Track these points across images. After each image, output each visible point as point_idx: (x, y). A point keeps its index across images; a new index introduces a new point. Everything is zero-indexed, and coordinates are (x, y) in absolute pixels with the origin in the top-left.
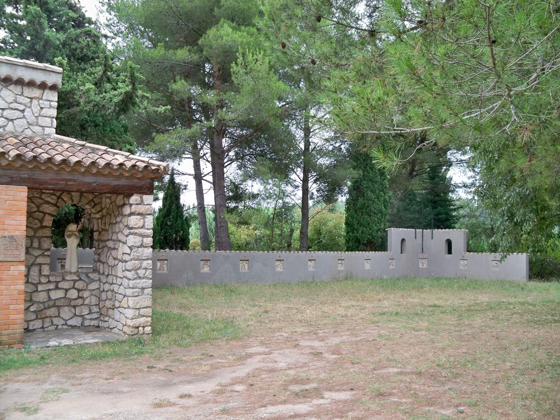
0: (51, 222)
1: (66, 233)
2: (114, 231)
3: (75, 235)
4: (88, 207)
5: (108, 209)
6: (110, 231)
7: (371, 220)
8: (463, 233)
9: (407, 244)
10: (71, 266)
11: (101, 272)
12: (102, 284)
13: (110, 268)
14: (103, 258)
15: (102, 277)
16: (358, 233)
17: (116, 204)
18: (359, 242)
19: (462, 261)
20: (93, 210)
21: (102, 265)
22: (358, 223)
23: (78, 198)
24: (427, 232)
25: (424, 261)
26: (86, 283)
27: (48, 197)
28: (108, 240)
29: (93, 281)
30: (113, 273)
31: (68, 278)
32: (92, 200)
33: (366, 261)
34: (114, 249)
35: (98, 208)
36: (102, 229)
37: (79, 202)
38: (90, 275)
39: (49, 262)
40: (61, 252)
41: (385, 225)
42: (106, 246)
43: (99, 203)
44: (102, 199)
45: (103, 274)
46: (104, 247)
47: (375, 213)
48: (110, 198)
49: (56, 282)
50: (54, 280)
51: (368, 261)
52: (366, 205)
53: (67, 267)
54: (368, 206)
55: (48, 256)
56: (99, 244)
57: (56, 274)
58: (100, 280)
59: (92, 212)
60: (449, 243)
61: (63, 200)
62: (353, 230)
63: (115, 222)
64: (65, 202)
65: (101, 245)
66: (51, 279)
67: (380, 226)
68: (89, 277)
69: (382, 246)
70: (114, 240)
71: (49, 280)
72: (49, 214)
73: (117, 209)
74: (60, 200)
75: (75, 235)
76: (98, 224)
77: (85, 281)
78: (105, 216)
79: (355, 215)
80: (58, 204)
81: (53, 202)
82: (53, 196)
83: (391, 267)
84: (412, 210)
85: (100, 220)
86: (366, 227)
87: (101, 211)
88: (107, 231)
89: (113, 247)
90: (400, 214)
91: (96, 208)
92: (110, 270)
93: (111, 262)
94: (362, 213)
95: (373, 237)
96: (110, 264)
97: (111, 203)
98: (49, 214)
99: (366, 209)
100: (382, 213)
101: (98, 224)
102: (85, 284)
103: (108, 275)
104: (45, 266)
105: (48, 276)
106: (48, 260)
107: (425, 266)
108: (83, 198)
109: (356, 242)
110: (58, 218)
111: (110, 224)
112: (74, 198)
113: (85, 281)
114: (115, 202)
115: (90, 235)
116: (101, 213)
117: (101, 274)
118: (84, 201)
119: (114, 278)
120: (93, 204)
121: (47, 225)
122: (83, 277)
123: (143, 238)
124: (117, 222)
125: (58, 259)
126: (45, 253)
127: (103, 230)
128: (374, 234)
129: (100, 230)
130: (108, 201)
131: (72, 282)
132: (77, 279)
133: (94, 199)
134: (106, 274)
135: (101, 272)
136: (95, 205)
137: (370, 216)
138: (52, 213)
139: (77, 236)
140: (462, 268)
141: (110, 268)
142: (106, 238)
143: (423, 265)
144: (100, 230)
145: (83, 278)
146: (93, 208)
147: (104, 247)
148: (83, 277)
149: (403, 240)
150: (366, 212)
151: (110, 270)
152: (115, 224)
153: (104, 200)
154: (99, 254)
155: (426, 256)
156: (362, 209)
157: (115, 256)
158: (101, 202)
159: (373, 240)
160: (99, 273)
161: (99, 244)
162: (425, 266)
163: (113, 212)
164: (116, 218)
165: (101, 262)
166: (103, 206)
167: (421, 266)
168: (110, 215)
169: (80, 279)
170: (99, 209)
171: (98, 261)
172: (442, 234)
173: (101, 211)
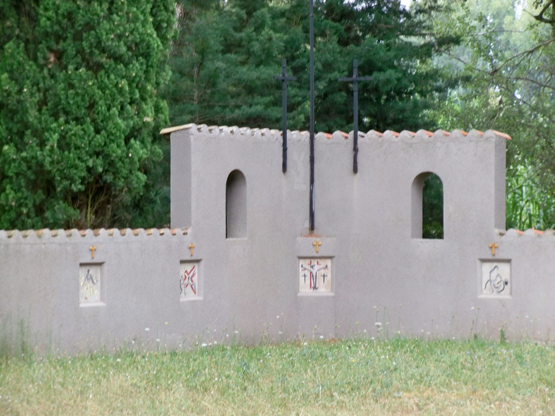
7: (102, 88)
8: (492, 146)
9: (252, 192)
16: (42, 144)
18: (49, 187)
19: (487, 267)
22: (43, 103)
24: (334, 143)
25: (318, 267)
33: (83, 272)
41: (158, 110)
47: (118, 58)
51: (93, 271)
52: (81, 19)
54: (89, 26)
60: (430, 189)
62: (21, 135)
67: (140, 113)
69: (147, 208)
79: (30, 67)
83: (188, 296)
84: (256, 47)
86: (77, 120)
90: (210, 66)
94: (59, 55)
95: (112, 164)
99: (78, 37)
100: (147, 56)
107: (324, 290)
109: (33, 186)
115: (536, 27)
125: (182, 262)
128: (116, 150)
137: (95, 68)
140: (486, 294)
143: (316, 285)
149: (234, 179)
150: (80, 52)
155: (327, 245)
156: (59, 38)
159: (109, 178)
162: (324, 290)
167: (305, 289)
172: (393, 157)
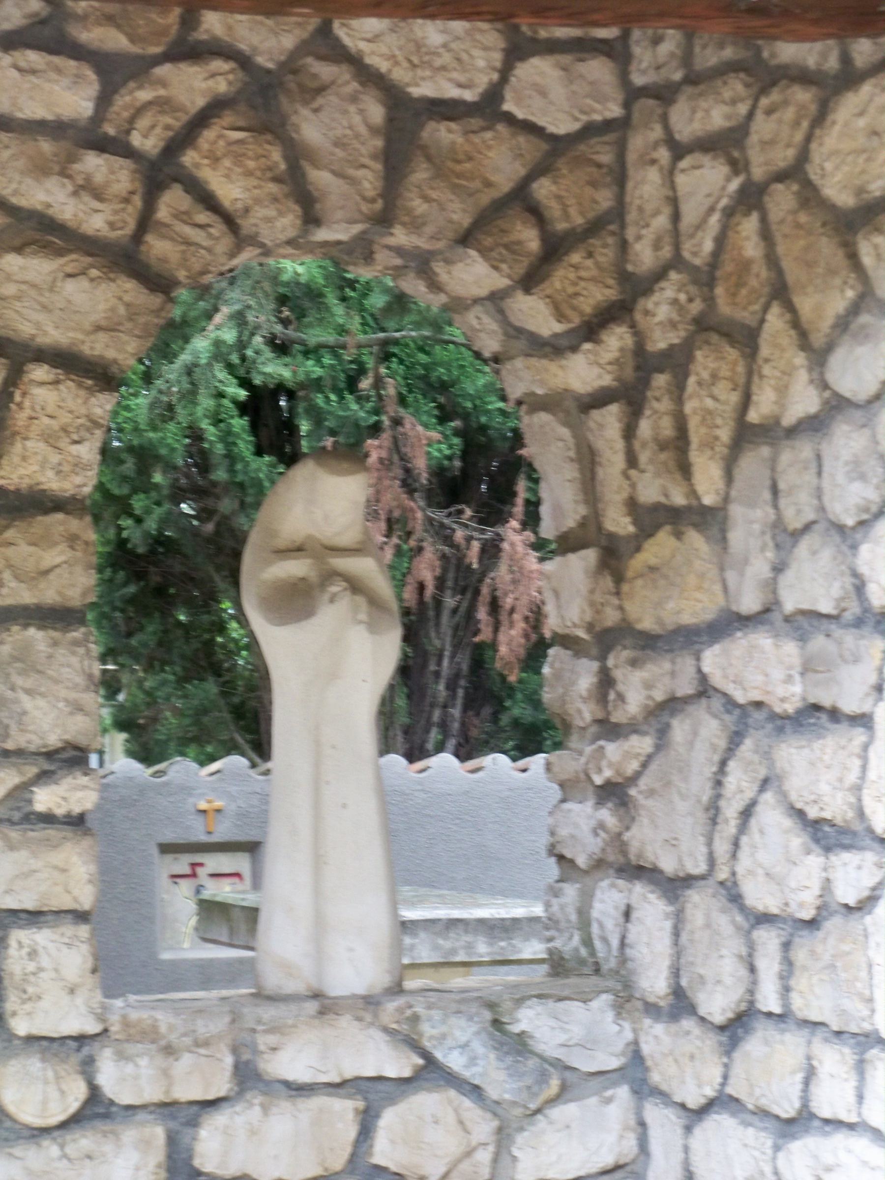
0: (88, 451)
1: (260, 572)
2: (797, 509)
3: (355, 586)
4: (473, 275)
5: (705, 279)
6: (747, 525)
10: (320, 928)
11: (655, 983)
12: (662, 1122)
13: (769, 941)
14: (668, 833)
15: (657, 1038)
17: (810, 196)
20: (535, 313)
21: (652, 909)
23: (370, 180)
26: (493, 1107)
27: (40, 169)
28: (728, 624)
29: (571, 1082)
30: (814, 999)
31: (293, 1061)
32: (520, 199)
34: (815, 716)
35: (585, 281)
36: (632, 505)
37: (384, 219)
38: (528, 1019)
39: (85, 896)
40: (187, 790)
42: (705, 689)
43: (595, 227)
44: (619, 177)
45: (680, 1004)
46: (672, 705)
48: (727, 144)
49: (167, 1108)
50: (152, 1093)
53: (284, 945)
55: (77, 822)
56: (606, 681)
57: (164, 1019)
58: (635, 1072)
59: (514, 332)
61: (208, 201)
63: (804, 401)
64: (229, 221)
65: (637, 688)
66: (116, 1078)
68: (518, 1046)
70: (806, 622)
71: (95, 1094)
72: (68, 362)
73: (828, 248)
74: (173, 201)
75: (355, 586)
76: (588, 460)
77: (475, 1091)
78: (677, 362)
80: (158, 247)
81: (96, 221)
82: (94, 163)
85: (609, 421)
87: (615, 312)
88: (708, 519)
89: (789, 695)
91: (560, 278)
92: (769, 966)
93: (780, 869)
96: (759, 896)
97: (751, 198)
98: (68, 362)
101: (588, 460)
102: (483, 1127)
103: (736, 1027)
104: (41, 937)
105: (78, 1049)
106: (70, 874)
108: (420, 174)
110: (151, 525)
111: (746, 434)
112: (320, 178)
113: (475, 1091)
114: (795, 172)
116: (616, 340)
117: (651, 1009)
118: (435, 207)
119: (833, 1061)
120: (530, 239)
121: (52, 483)
122: (460, 1044)
123: (802, 639)
124: (836, 405)
125: (167, 849)
126: (45, 799)
127: (652, 519)
129: (619, 523)
130: (706, 182)
131: (344, 1111)
132: (397, 1064)
133: (543, 190)
134: (718, 1004)
135: (655, 983)
136: (554, 249)
138: (98, 347)
139: (374, 602)
141: (769, 941)
142: (694, 606)
144: (619, 523)
145: (455, 1061)
146: (529, 282)
147: (672, 705)
148: (460, 1044)
151: (769, 966)
152: (815, 425)
153: (647, 186)
154: (614, 793)
157: (834, 806)
158: (618, 213)
160: (627, 999)
161: (606, 681)
163: (781, 292)
164: (819, 357)
165: (638, 871)
166: (645, 256)
168: (747, 340)
169: (431, 1072)
170: (597, 295)
171: (599, 864)
173: (615, 312)
